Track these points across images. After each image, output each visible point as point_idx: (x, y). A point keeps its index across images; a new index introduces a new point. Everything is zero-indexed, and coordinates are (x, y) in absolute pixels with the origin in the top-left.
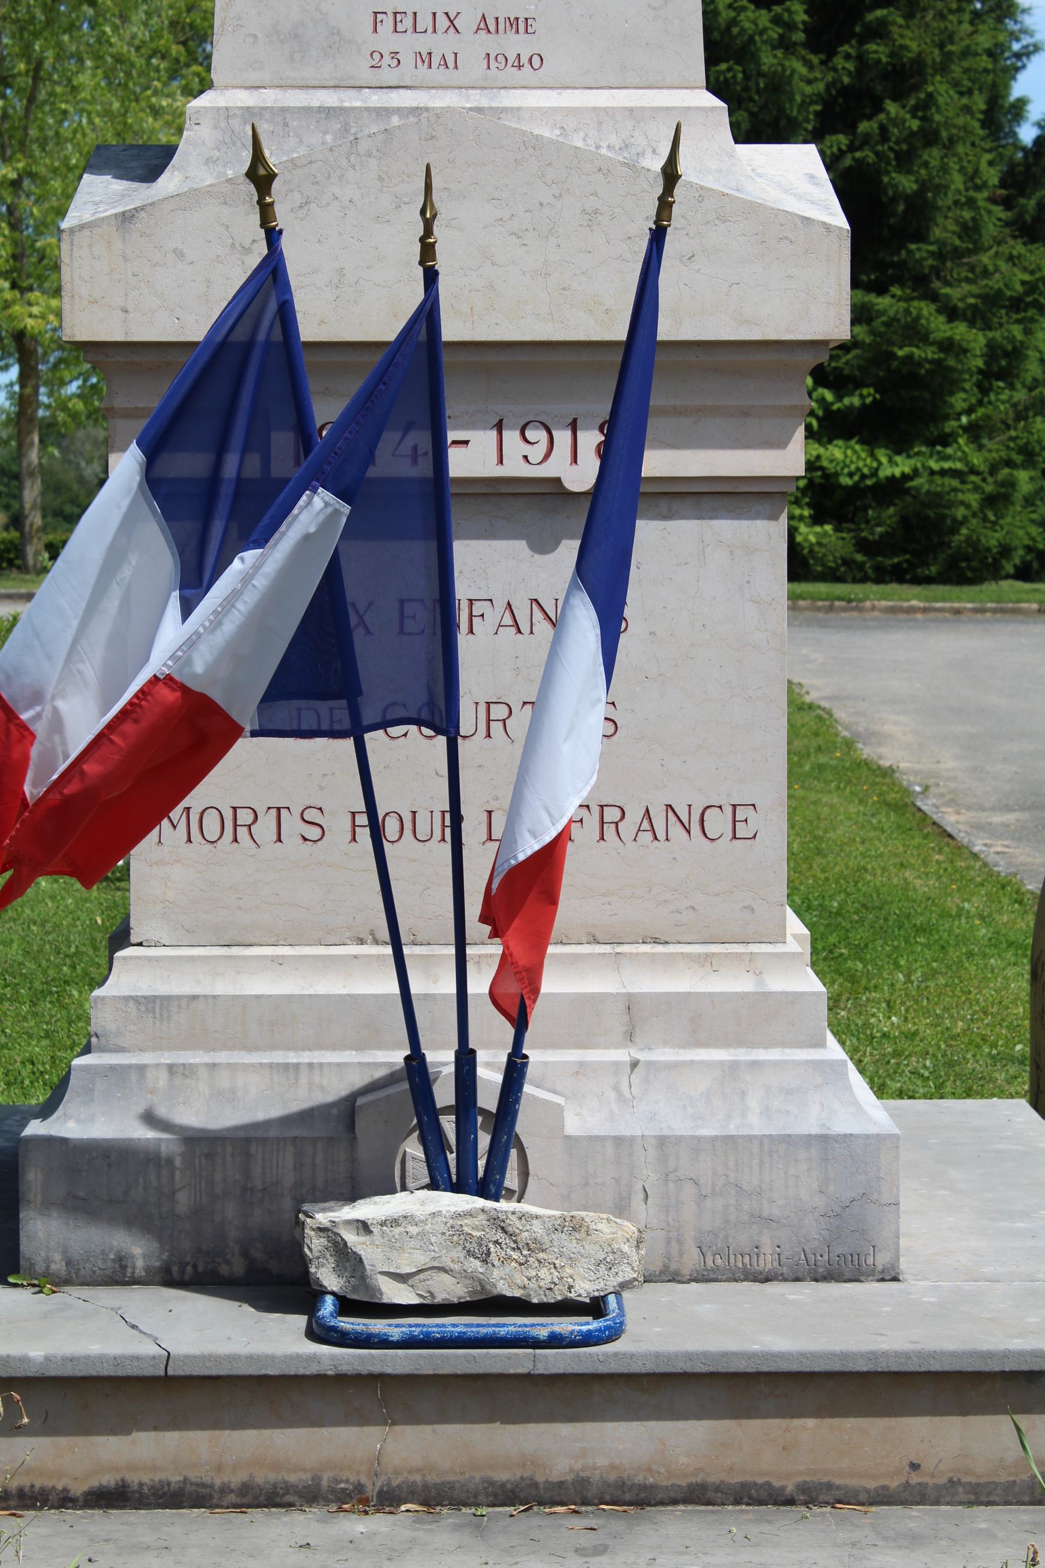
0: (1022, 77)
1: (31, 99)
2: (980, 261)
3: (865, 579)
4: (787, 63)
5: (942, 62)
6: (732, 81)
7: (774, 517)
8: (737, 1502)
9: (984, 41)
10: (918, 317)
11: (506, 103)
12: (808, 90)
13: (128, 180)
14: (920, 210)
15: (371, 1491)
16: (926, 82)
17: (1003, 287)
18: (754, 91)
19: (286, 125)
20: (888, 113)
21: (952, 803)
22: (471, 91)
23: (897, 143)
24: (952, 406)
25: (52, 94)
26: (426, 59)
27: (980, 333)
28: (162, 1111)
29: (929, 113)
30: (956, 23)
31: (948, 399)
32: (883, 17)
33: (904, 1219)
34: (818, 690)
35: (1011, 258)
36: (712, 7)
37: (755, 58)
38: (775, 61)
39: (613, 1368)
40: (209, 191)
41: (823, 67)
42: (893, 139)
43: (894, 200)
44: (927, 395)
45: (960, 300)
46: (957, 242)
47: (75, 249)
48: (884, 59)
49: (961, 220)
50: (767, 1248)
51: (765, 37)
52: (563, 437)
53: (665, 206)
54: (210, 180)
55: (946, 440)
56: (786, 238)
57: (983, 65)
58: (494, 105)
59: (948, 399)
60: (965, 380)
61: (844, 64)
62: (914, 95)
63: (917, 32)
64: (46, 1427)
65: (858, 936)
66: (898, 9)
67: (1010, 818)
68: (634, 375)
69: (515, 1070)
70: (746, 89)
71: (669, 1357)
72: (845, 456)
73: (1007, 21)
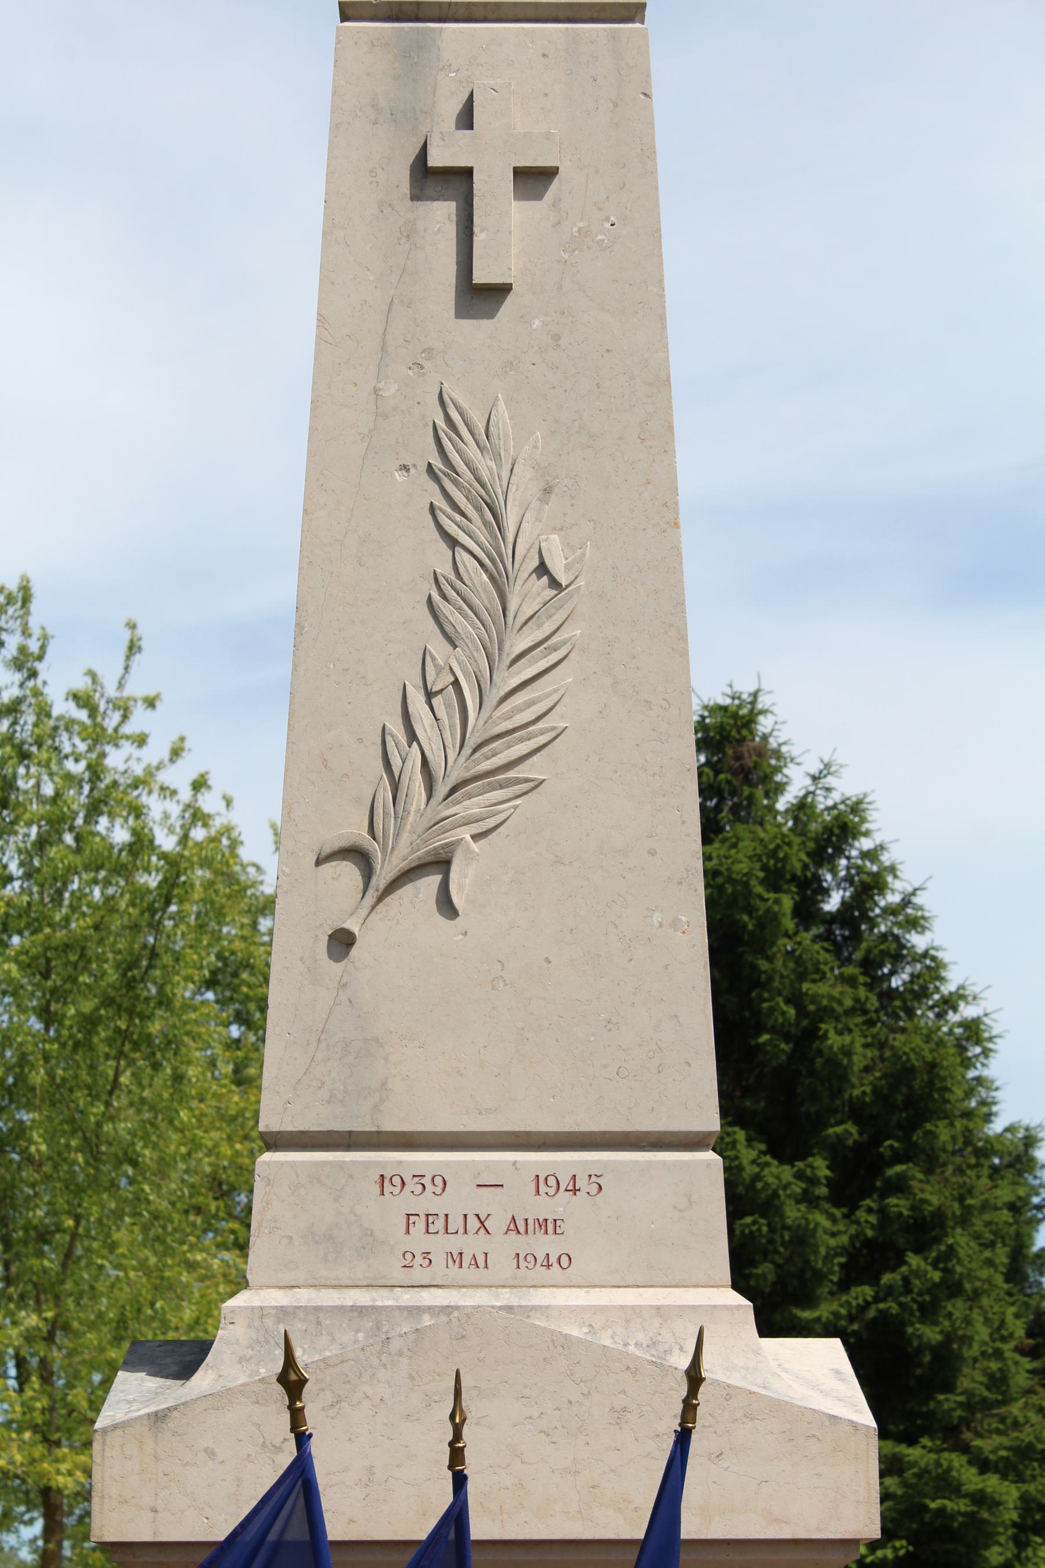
2: (1010, 1413)
4: (810, 1217)
5: (962, 1215)
6: (757, 1234)
9: (1004, 1194)
10: (949, 1469)
11: (536, 1302)
12: (832, 1242)
13: (162, 1377)
14: (945, 1362)
16: (946, 1235)
17: (1034, 1441)
18: (779, 1244)
19: (319, 1323)
20: (910, 1265)
22: (500, 1290)
23: (920, 1294)
24: (987, 1560)
25: (88, 1250)
26: (457, 1259)
27: (1013, 1486)
29: (950, 1265)
30: (974, 1178)
31: (982, 1552)
32: (903, 1172)
36: (736, 1163)
37: (779, 1212)
38: (798, 1215)
41: (847, 1221)
42: (916, 1290)
43: (920, 1350)
44: (961, 1549)
45: (992, 1452)
46: (986, 1393)
47: (107, 1449)
48: (906, 1213)
49: (989, 1371)
51: (788, 1192)
53: (689, 1408)
54: (242, 1379)
56: (814, 1436)
57: (1004, 1218)
58: (524, 1303)
59: (982, 1552)
60: (999, 1534)
61: (866, 1218)
62: (935, 1247)
63: (936, 1187)
66: (916, 1164)
70: (771, 1241)
73: (1026, 1175)
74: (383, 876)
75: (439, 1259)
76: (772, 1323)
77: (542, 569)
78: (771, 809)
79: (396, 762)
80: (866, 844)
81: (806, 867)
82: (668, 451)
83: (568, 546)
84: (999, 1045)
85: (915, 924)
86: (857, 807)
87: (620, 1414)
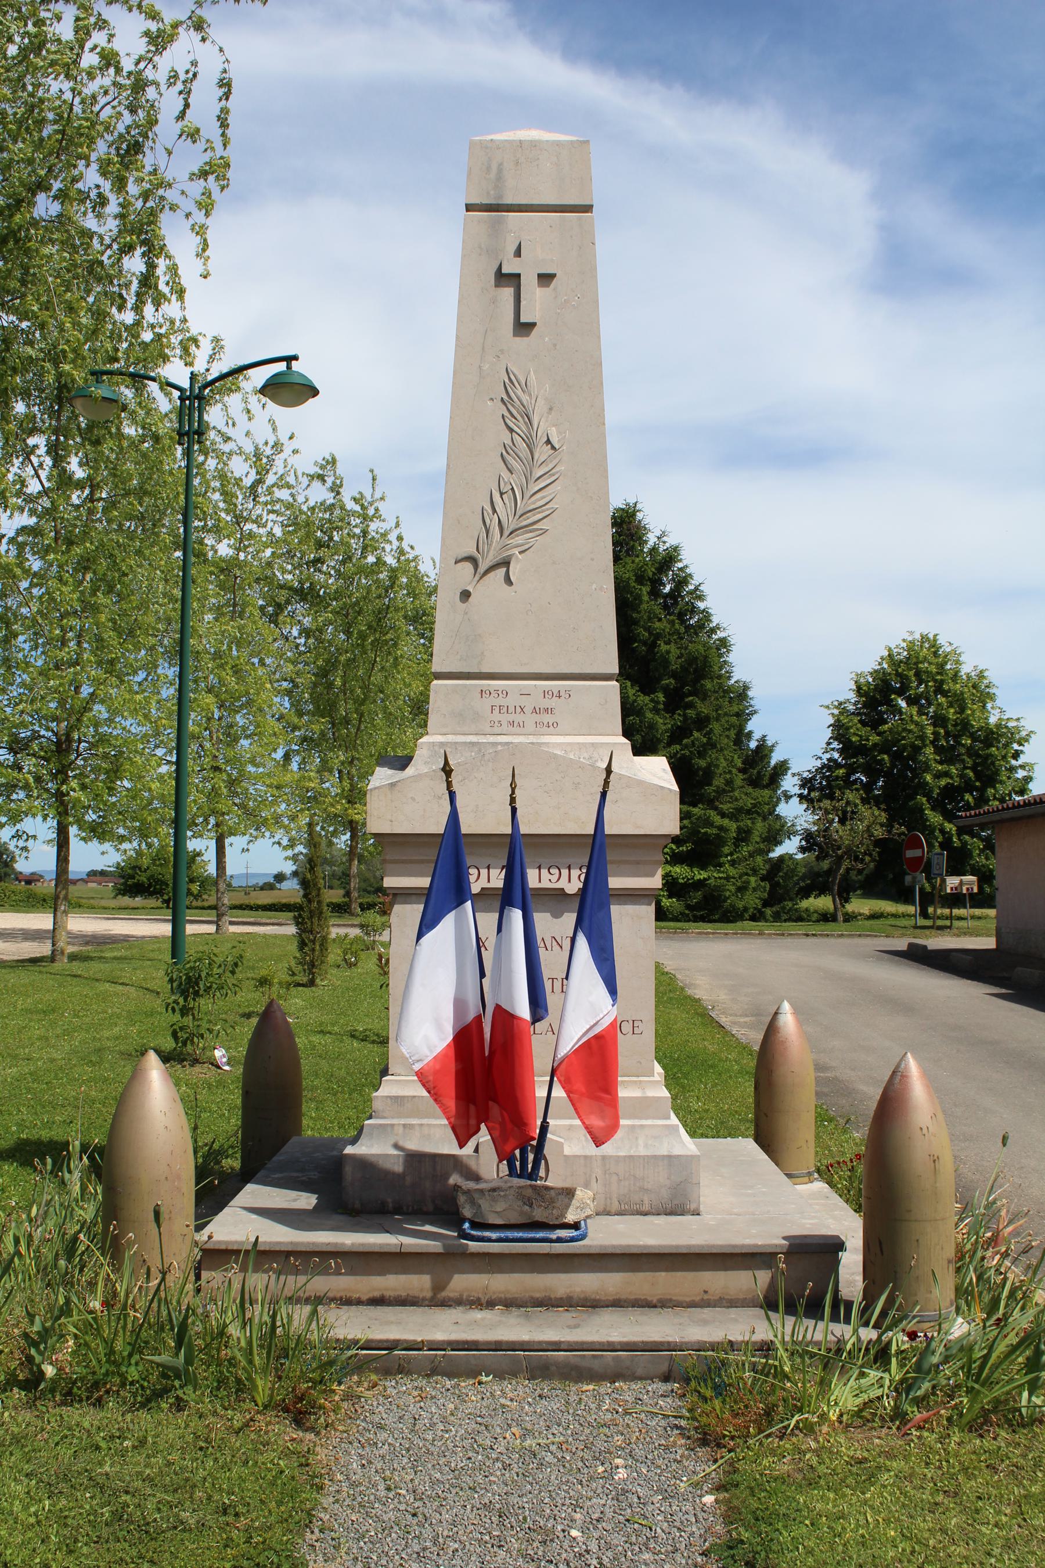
0: (749, 723)
1: (358, 729)
3: (689, 921)
7: (650, 904)
8: (633, 1306)
14: (708, 775)
15: (484, 1301)
21: (723, 1013)
28: (401, 1143)
33: (702, 1189)
34: (669, 966)
35: (746, 794)
37: (643, 715)
39: (583, 1251)
40: (426, 775)
50: (646, 1202)
52: (565, 872)
53: (606, 783)
55: (721, 865)
61: (678, 718)
64: (352, 1272)
65: (685, 1069)
67: (747, 1019)
68: (597, 849)
69: (544, 1128)
71: (605, 1247)
72: (680, 871)
74: (482, 568)
75: (505, 723)
76: (639, 750)
77: (548, 442)
78: (642, 550)
79: (488, 521)
80: (680, 565)
81: (654, 574)
82: (601, 393)
83: (559, 433)
84: (733, 648)
85: (701, 598)
86: (676, 549)
87: (576, 786)
